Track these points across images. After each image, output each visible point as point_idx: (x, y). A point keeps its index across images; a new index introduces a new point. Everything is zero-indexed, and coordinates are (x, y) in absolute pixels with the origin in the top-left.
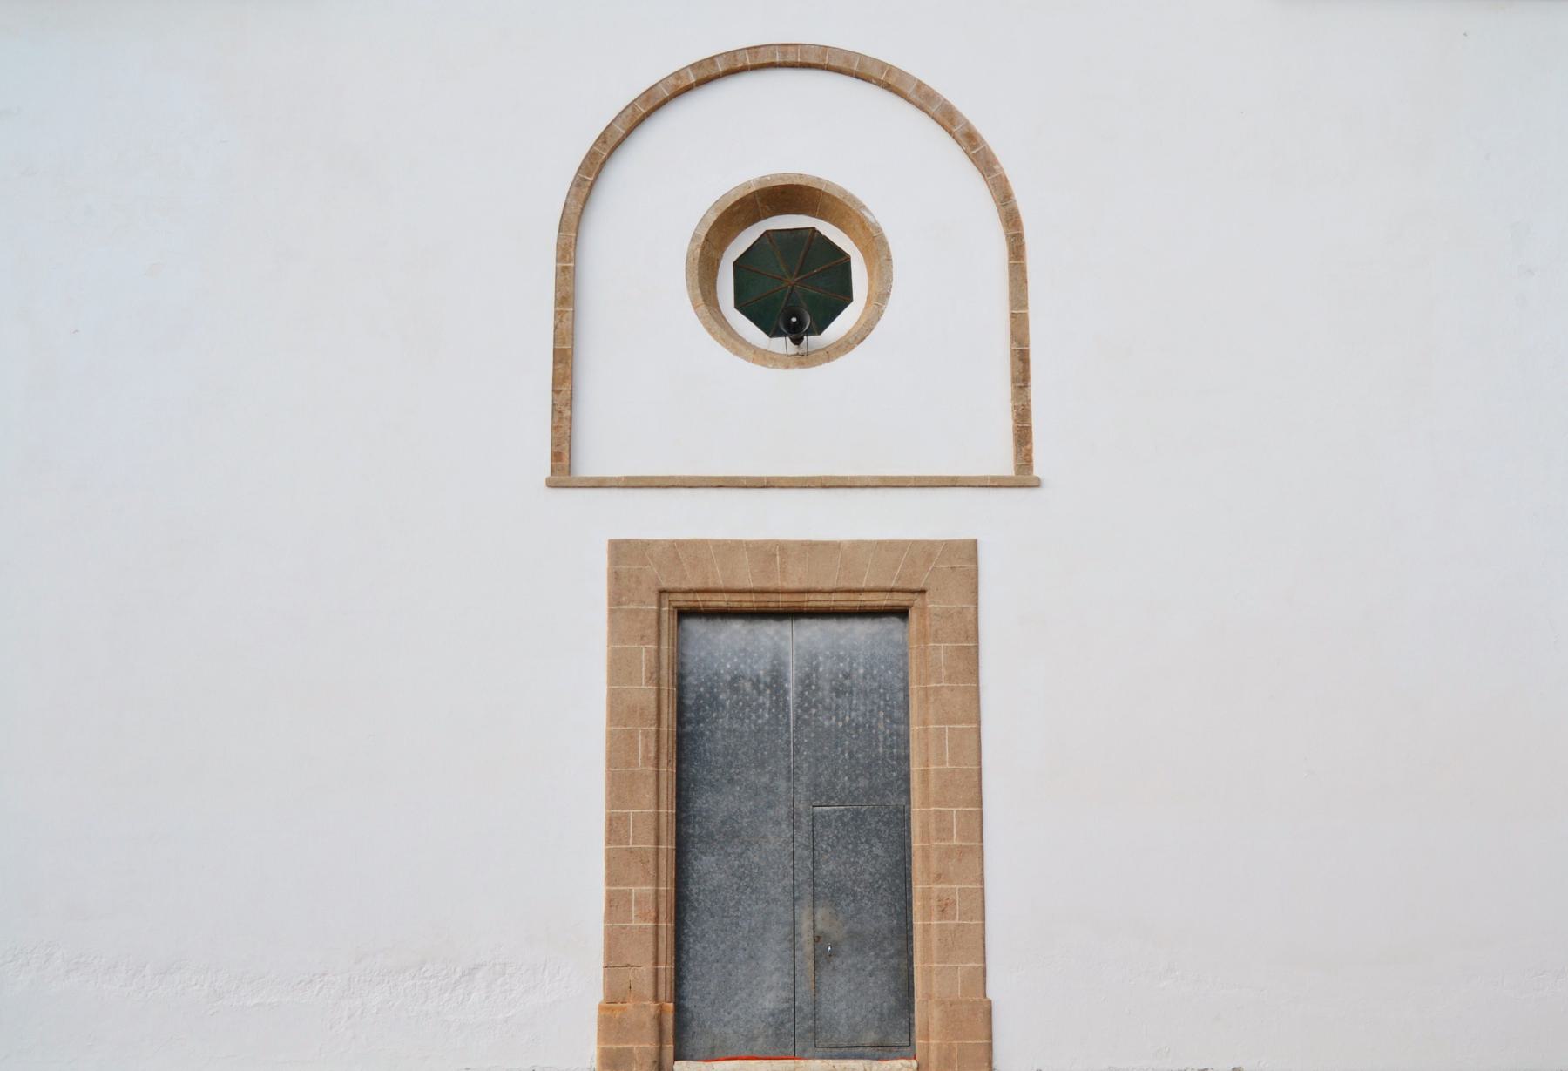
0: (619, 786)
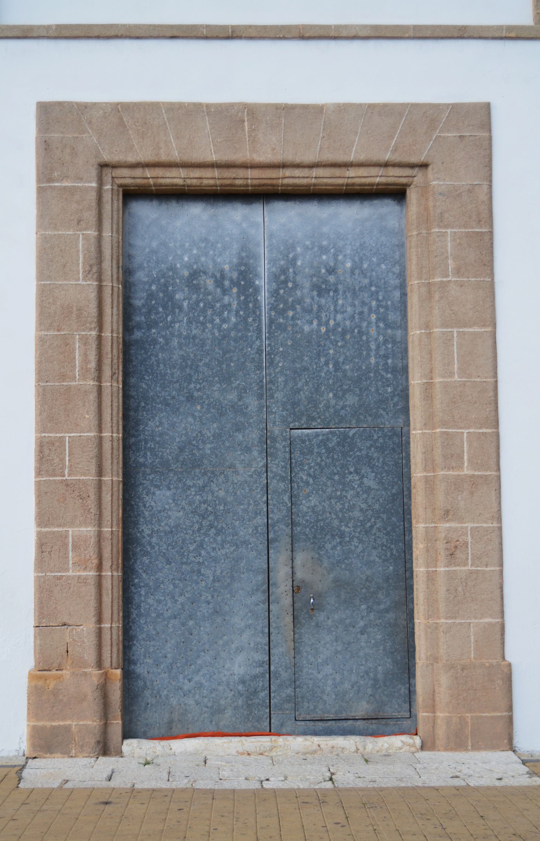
0: (52, 404)
